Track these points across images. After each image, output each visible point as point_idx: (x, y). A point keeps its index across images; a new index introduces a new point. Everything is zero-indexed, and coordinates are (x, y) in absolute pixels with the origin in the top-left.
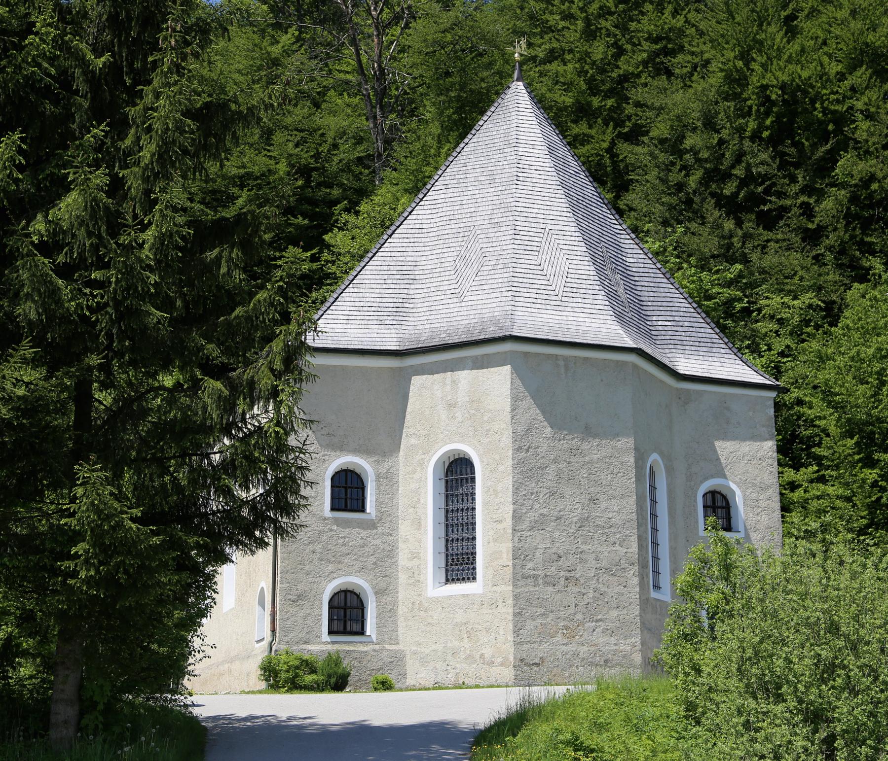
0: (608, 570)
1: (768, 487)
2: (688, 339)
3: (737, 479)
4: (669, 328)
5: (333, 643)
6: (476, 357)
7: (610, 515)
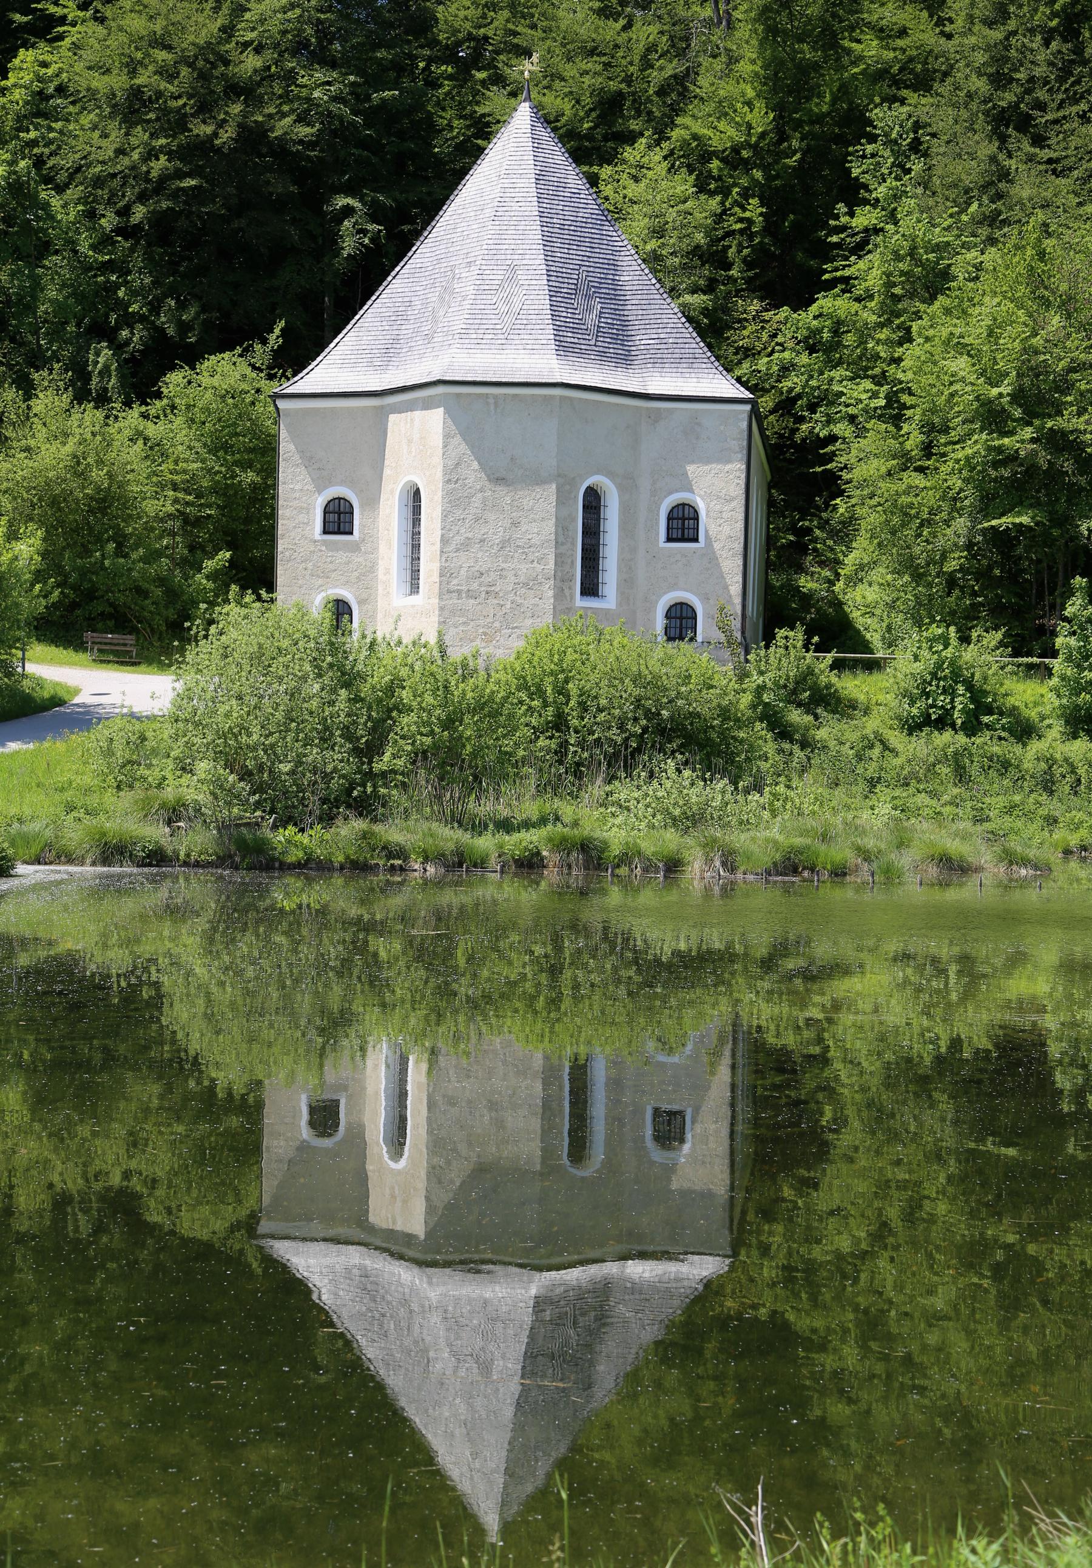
0: (526, 584)
1: (732, 499)
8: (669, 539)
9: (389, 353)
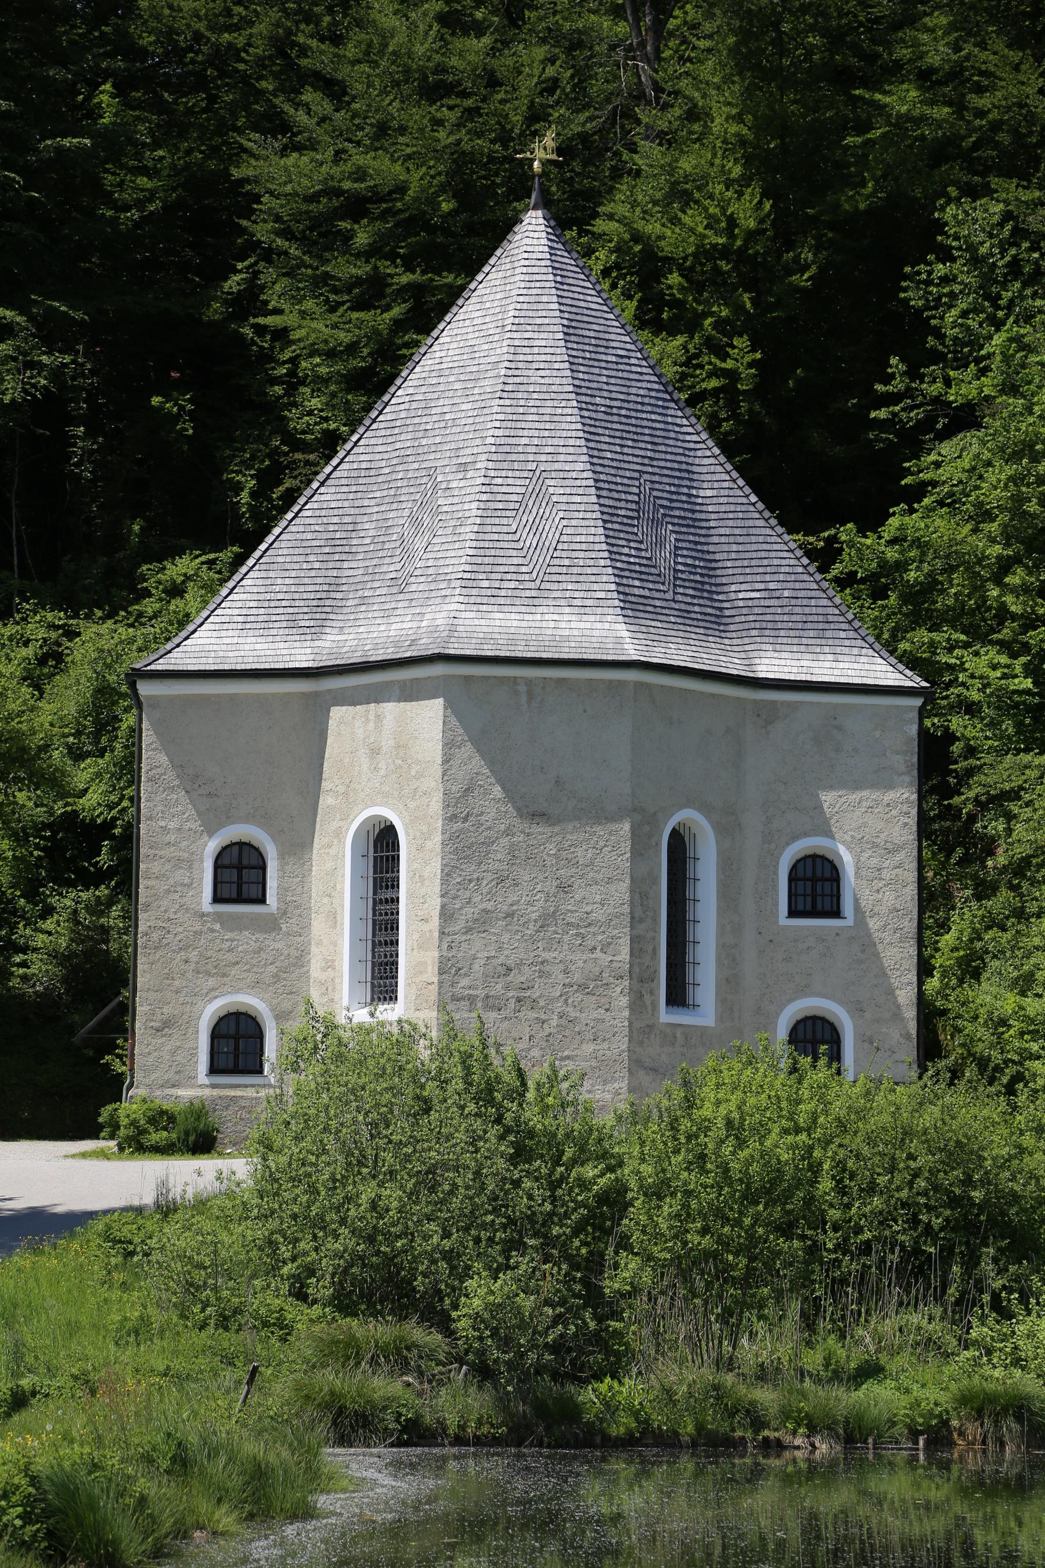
0: (582, 987)
2: (786, 618)
3: (847, 838)
4: (756, 603)
5: (213, 1086)
6: (404, 681)
7: (589, 909)
8: (793, 913)
9: (321, 608)
